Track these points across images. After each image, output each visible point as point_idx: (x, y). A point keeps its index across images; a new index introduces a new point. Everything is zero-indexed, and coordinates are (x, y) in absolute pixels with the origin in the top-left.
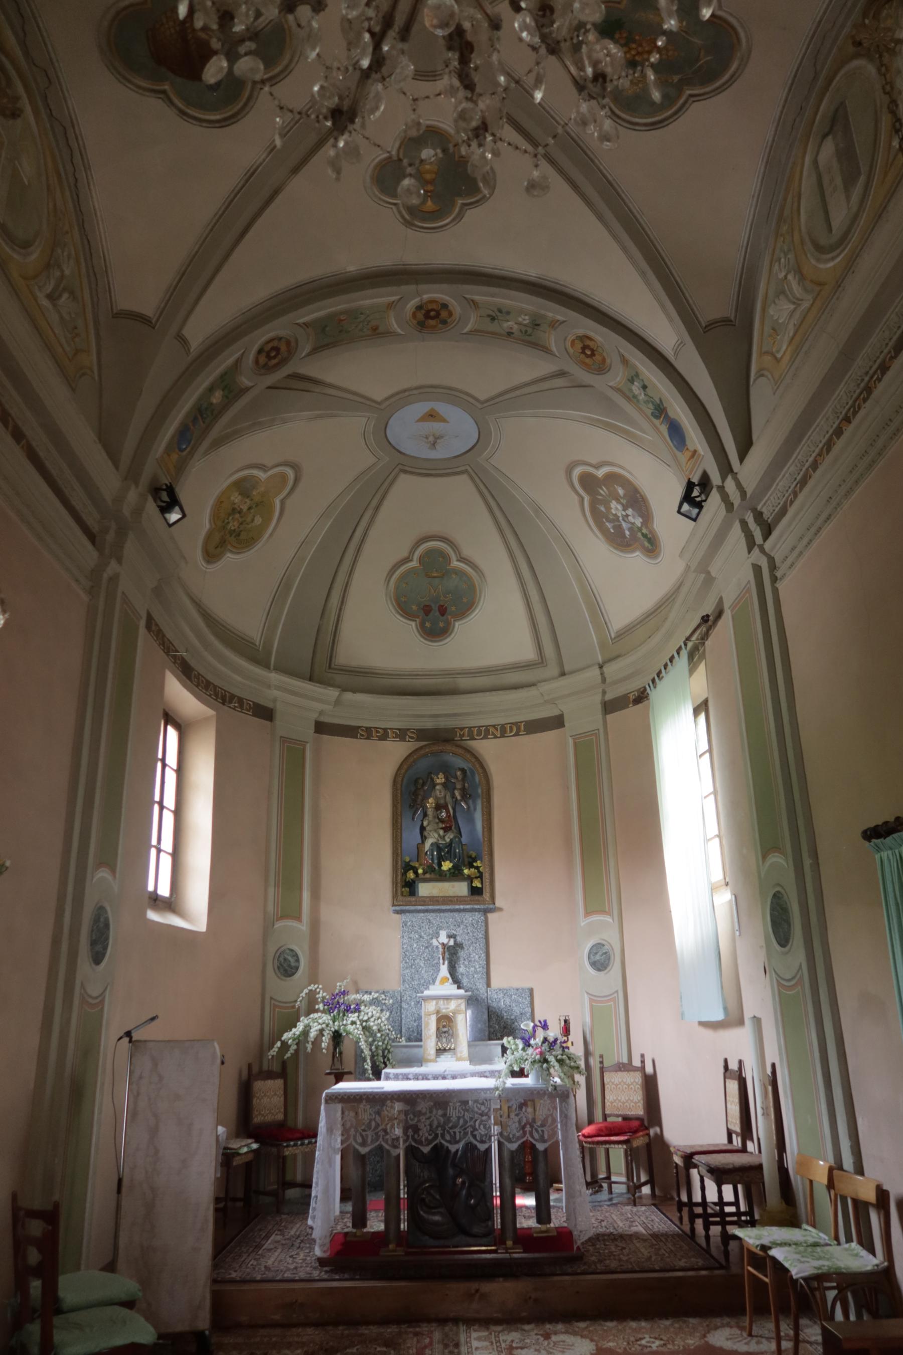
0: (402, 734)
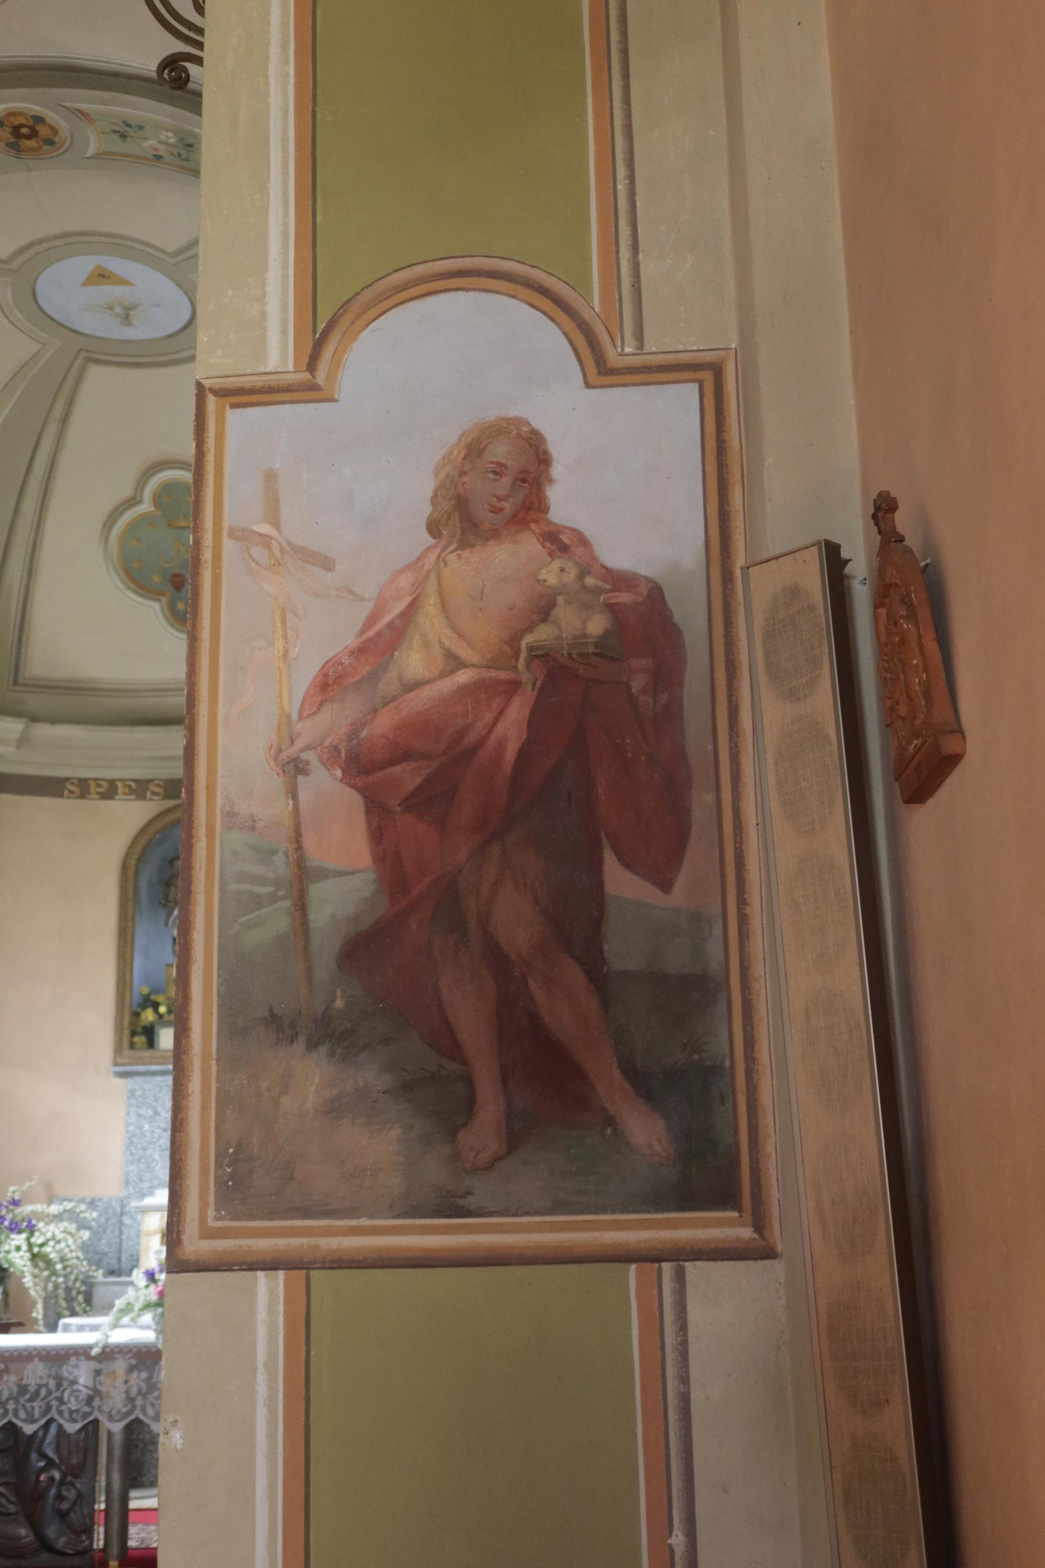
0: (140, 789)
